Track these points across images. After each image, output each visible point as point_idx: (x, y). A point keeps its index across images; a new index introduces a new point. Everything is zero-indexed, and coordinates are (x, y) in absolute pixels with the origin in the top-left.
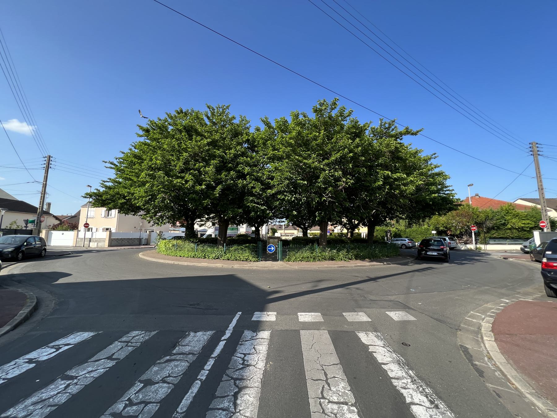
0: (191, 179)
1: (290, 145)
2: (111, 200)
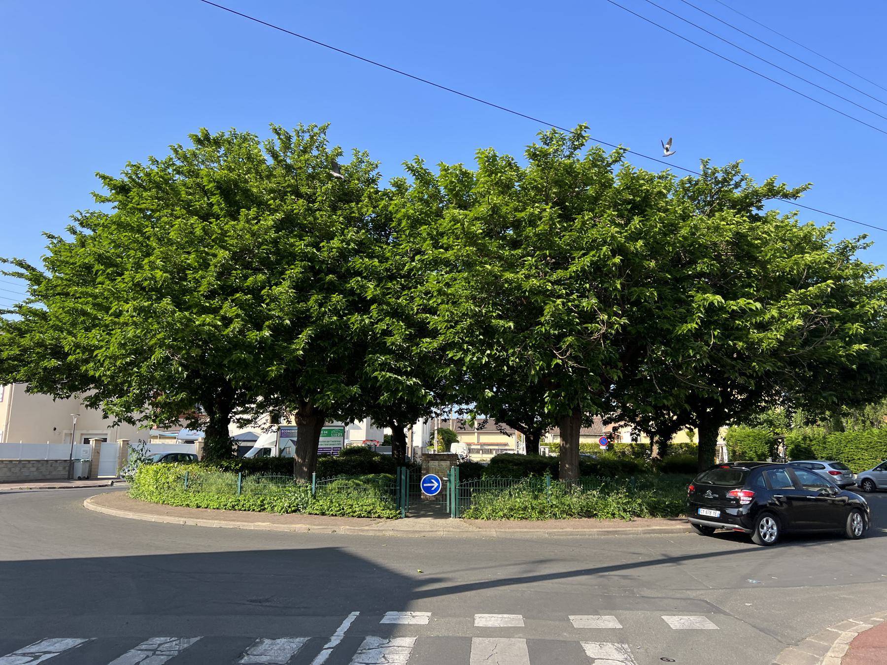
0: (238, 316)
1: (471, 239)
2: (21, 361)
